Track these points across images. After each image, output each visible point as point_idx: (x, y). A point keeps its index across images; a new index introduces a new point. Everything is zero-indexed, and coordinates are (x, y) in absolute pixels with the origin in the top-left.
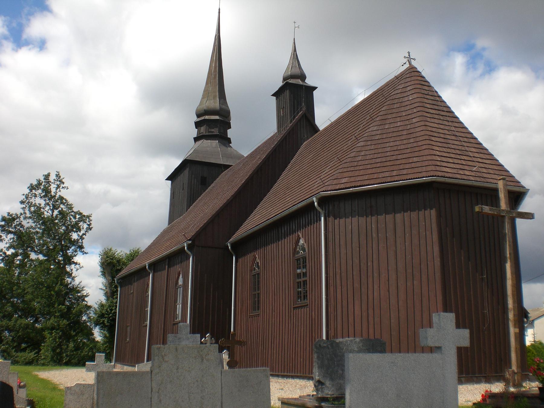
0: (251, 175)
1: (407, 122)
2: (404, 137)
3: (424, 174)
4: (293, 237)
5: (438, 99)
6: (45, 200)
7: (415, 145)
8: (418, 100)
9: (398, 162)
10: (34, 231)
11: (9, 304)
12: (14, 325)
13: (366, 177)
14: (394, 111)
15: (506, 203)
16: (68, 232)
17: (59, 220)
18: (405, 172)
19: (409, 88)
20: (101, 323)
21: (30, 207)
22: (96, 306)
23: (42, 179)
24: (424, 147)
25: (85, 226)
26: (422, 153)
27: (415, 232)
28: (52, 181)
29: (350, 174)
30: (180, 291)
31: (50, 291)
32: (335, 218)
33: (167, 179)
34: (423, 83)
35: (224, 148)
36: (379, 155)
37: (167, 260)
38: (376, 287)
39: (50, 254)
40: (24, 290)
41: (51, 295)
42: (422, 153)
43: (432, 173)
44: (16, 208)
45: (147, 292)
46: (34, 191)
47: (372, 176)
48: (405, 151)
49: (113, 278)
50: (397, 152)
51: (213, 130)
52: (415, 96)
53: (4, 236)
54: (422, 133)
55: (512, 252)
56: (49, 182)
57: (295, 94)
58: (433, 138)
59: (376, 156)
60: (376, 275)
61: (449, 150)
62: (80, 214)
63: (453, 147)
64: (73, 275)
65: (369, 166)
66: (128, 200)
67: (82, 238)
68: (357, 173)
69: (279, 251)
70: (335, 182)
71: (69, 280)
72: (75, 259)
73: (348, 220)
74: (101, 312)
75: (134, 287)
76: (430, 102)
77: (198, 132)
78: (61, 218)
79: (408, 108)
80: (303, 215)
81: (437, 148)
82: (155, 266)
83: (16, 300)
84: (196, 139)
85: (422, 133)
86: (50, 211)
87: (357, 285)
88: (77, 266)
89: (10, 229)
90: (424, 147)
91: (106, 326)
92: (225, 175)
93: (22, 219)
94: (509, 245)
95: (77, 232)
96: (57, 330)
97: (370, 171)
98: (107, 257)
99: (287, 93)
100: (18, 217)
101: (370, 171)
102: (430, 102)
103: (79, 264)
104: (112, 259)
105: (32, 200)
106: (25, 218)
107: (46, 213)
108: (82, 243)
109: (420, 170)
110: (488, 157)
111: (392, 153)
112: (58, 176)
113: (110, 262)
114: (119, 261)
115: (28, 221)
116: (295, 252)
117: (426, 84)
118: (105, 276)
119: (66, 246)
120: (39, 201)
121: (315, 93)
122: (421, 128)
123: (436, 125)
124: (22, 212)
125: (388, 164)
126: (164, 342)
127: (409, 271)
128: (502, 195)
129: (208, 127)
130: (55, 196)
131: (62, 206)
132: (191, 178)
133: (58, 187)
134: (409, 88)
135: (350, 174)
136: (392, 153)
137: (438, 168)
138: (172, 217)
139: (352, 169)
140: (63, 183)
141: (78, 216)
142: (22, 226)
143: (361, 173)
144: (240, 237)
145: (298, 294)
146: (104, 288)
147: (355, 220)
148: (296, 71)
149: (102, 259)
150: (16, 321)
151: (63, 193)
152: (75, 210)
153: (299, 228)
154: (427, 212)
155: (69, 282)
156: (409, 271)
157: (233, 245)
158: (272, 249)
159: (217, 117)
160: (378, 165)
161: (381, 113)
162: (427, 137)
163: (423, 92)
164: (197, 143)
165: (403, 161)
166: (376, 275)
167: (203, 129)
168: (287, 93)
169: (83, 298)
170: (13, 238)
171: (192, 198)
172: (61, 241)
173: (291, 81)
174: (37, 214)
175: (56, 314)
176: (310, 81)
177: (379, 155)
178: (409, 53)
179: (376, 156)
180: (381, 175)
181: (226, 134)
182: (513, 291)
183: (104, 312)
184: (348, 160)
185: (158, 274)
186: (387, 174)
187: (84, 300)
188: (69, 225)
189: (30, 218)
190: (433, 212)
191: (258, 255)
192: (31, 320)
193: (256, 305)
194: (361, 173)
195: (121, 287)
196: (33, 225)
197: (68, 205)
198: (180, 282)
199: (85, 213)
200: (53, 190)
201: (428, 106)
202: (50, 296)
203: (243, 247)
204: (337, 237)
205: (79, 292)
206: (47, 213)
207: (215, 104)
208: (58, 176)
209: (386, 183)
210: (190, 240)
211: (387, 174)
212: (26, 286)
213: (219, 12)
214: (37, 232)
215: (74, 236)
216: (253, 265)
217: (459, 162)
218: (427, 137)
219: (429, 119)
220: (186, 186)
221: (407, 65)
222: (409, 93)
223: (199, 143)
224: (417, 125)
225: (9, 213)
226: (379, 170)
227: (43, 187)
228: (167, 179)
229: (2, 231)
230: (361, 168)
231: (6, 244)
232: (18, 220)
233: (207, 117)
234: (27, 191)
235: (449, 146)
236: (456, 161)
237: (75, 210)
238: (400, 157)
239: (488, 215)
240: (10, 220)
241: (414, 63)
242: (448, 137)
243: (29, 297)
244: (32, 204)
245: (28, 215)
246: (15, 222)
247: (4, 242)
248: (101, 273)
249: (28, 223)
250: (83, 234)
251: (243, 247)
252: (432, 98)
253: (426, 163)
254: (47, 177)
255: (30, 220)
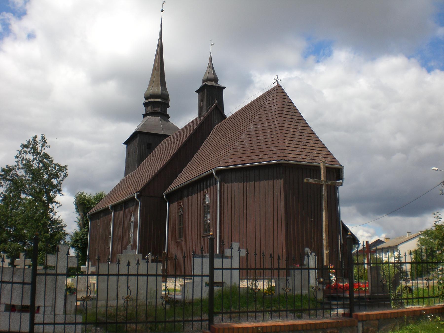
0: (179, 148)
1: (271, 124)
2: (268, 134)
3: (277, 158)
4: (202, 193)
5: (292, 107)
6: (33, 156)
7: (274, 139)
8: (280, 109)
9: (263, 150)
10: (25, 178)
11: (5, 232)
12: (9, 248)
13: (244, 159)
14: (264, 115)
15: (324, 177)
16: (50, 178)
17: (44, 170)
18: (266, 156)
19: (275, 101)
20: (76, 247)
21: (22, 161)
22: (72, 234)
23: (31, 140)
24: (279, 141)
25: (63, 174)
26: (277, 145)
27: (271, 193)
28: (39, 142)
29: (235, 156)
30: (132, 225)
31: (38, 223)
32: (225, 183)
33: (123, 144)
34: (284, 97)
35: (164, 122)
36: (253, 145)
37: (123, 204)
38: (248, 225)
39: (37, 196)
40: (16, 221)
41: (39, 226)
42: (277, 145)
43: (281, 158)
44: (12, 162)
45: (110, 225)
46: (25, 149)
47: (247, 158)
48: (268, 143)
49: (85, 214)
50: (263, 144)
51: (156, 109)
52: (278, 106)
53: (3, 183)
54: (279, 131)
55: (326, 205)
56: (36, 142)
57: (211, 93)
58: (285, 135)
59: (251, 145)
60: (248, 218)
61: (294, 142)
62: (59, 166)
63: (297, 140)
64: (54, 211)
65: (246, 152)
66: (94, 155)
67: (60, 183)
68: (239, 156)
69: (193, 200)
70: (226, 161)
71: (52, 215)
72: (56, 199)
73: (233, 184)
74: (76, 238)
75: (101, 221)
76: (287, 110)
77: (146, 110)
78: (45, 169)
79: (273, 114)
80: (206, 181)
81: (287, 142)
82: (115, 207)
83: (9, 229)
84: (144, 116)
85: (279, 131)
86: (37, 164)
87: (237, 224)
88: (58, 205)
89: (8, 178)
90: (279, 141)
91: (80, 248)
92: (164, 143)
93: (17, 170)
94: (325, 202)
95: (56, 178)
96: (44, 251)
97: (246, 155)
98: (80, 199)
99: (205, 91)
100: (14, 168)
101: (246, 155)
102: (287, 110)
103: (59, 203)
104: (84, 200)
105: (24, 155)
106: (19, 169)
107: (34, 165)
108: (60, 187)
109: (274, 155)
110: (320, 146)
111: (261, 144)
112: (43, 138)
113: (83, 202)
114: (89, 201)
115: (20, 170)
116: (179, 211)
117: (286, 97)
118: (79, 212)
119: (49, 190)
120: (30, 157)
121: (224, 91)
122: (279, 128)
123: (289, 126)
124: (16, 164)
125: (257, 151)
126: (122, 253)
127: (267, 215)
128: (322, 172)
129: (153, 107)
130: (40, 153)
131: (45, 160)
132: (141, 144)
133: (43, 146)
134: (275, 101)
135: (235, 156)
136: (261, 144)
137: (285, 155)
138: (127, 171)
139: (236, 153)
140: (46, 143)
141: (57, 168)
142: (17, 175)
143: (242, 156)
144: (171, 191)
145: (180, 230)
146: (78, 221)
147: (237, 184)
148: (212, 76)
149: (76, 200)
150: (10, 245)
151: (46, 150)
152: (55, 162)
153: (206, 187)
154: (278, 181)
155: (51, 216)
156: (267, 215)
157: (166, 195)
158: (190, 199)
159: (159, 100)
160: (252, 151)
161: (257, 117)
162: (281, 134)
163: (283, 103)
164: (145, 118)
165: (266, 150)
166: (248, 218)
167: (149, 108)
168: (205, 91)
169: (62, 228)
170: (10, 184)
171: (141, 159)
172: (45, 186)
173: (208, 83)
174: (27, 166)
175: (43, 240)
176: (221, 83)
177: (253, 145)
178: (277, 76)
179: (251, 145)
180: (252, 158)
181: (166, 111)
182: (326, 229)
183: (78, 238)
184: (234, 147)
185: (117, 213)
186: (256, 157)
187: (62, 229)
188: (51, 173)
189: (22, 168)
190: (282, 181)
191: (182, 202)
192: (20, 244)
193: (181, 235)
194: (242, 156)
195: (91, 221)
196: (25, 174)
197: (49, 158)
198: (132, 219)
199: (62, 165)
200: (39, 148)
201: (285, 113)
202: (38, 227)
203: (174, 196)
204: (226, 194)
205: (59, 223)
206: (35, 166)
207: (158, 90)
208: (43, 138)
209: (255, 163)
210: (138, 192)
211: (256, 157)
212: (17, 219)
213: (162, 22)
214: (28, 180)
215: (55, 181)
216: (179, 209)
217: (300, 150)
218: (281, 134)
219: (284, 122)
220: (137, 151)
221: (276, 84)
222: (274, 104)
223: (147, 118)
224: (277, 126)
225: (7, 166)
226: (251, 155)
227: (32, 146)
228: (123, 144)
229: (2, 179)
230: (242, 152)
231: (5, 188)
232: (14, 171)
233: (152, 100)
234: (20, 149)
235: (295, 139)
236: (298, 149)
237: (55, 162)
238: (264, 146)
239: (311, 184)
240: (7, 171)
241: (280, 83)
242: (296, 133)
243: (20, 227)
244: (23, 158)
245: (21, 166)
246: (12, 172)
247: (3, 187)
248: (75, 210)
249: (21, 173)
250: (61, 180)
251: (174, 196)
252: (289, 107)
253: (279, 151)
254: (35, 138)
255: (22, 170)
